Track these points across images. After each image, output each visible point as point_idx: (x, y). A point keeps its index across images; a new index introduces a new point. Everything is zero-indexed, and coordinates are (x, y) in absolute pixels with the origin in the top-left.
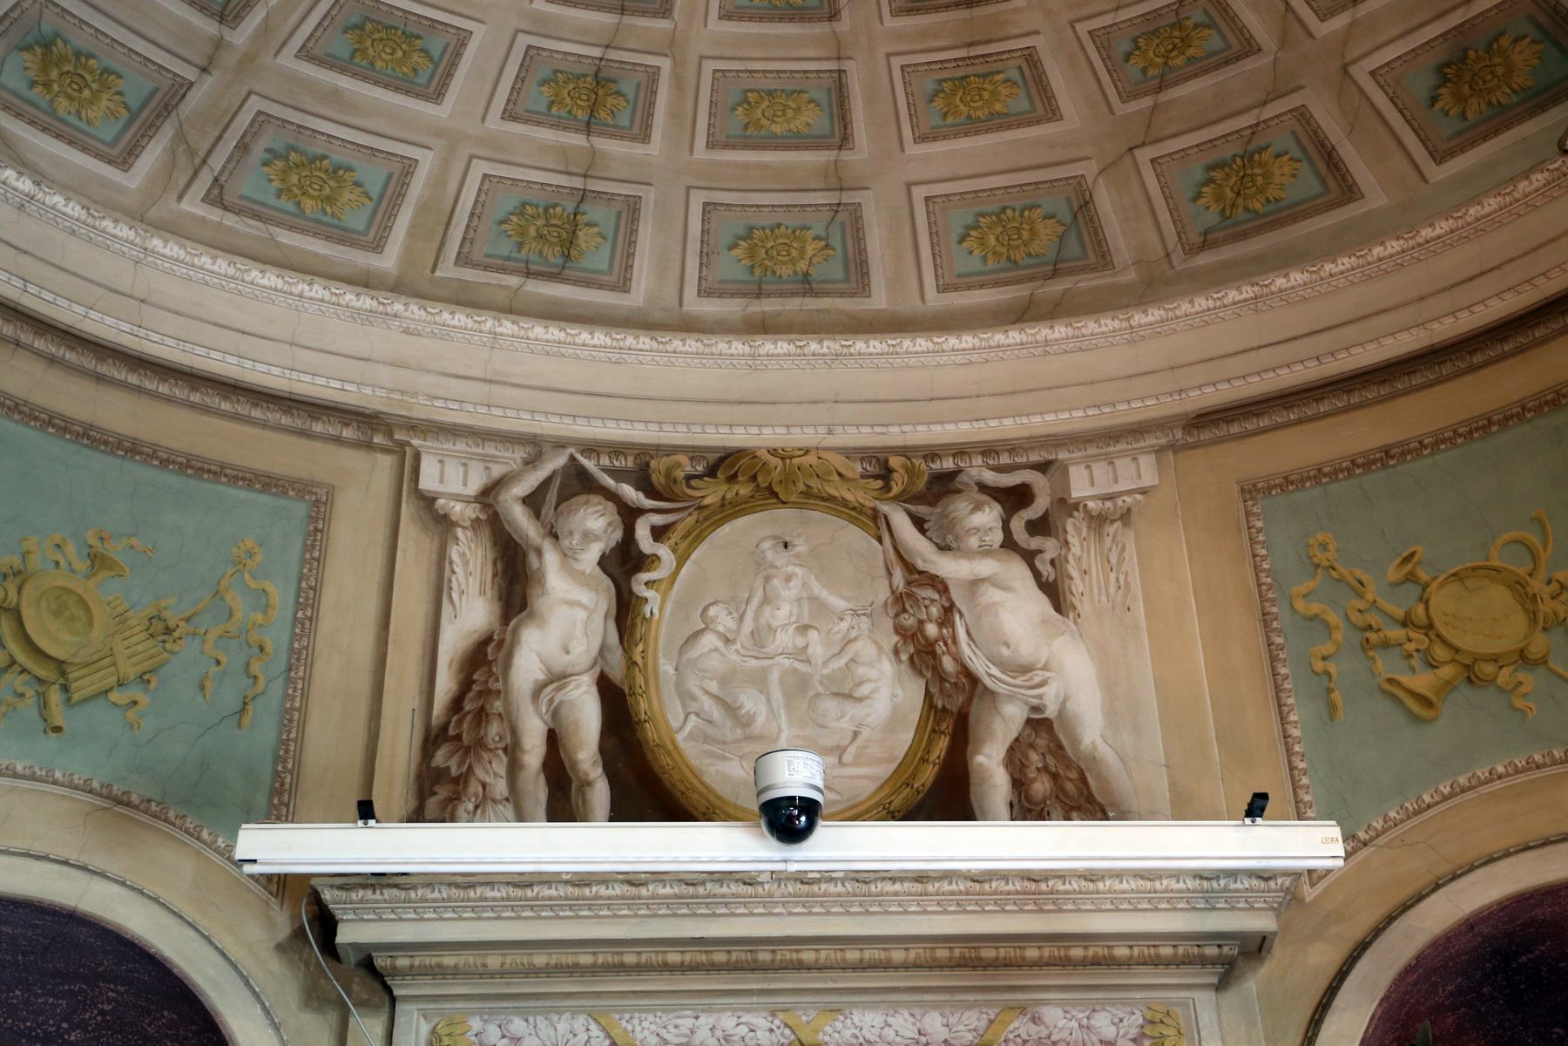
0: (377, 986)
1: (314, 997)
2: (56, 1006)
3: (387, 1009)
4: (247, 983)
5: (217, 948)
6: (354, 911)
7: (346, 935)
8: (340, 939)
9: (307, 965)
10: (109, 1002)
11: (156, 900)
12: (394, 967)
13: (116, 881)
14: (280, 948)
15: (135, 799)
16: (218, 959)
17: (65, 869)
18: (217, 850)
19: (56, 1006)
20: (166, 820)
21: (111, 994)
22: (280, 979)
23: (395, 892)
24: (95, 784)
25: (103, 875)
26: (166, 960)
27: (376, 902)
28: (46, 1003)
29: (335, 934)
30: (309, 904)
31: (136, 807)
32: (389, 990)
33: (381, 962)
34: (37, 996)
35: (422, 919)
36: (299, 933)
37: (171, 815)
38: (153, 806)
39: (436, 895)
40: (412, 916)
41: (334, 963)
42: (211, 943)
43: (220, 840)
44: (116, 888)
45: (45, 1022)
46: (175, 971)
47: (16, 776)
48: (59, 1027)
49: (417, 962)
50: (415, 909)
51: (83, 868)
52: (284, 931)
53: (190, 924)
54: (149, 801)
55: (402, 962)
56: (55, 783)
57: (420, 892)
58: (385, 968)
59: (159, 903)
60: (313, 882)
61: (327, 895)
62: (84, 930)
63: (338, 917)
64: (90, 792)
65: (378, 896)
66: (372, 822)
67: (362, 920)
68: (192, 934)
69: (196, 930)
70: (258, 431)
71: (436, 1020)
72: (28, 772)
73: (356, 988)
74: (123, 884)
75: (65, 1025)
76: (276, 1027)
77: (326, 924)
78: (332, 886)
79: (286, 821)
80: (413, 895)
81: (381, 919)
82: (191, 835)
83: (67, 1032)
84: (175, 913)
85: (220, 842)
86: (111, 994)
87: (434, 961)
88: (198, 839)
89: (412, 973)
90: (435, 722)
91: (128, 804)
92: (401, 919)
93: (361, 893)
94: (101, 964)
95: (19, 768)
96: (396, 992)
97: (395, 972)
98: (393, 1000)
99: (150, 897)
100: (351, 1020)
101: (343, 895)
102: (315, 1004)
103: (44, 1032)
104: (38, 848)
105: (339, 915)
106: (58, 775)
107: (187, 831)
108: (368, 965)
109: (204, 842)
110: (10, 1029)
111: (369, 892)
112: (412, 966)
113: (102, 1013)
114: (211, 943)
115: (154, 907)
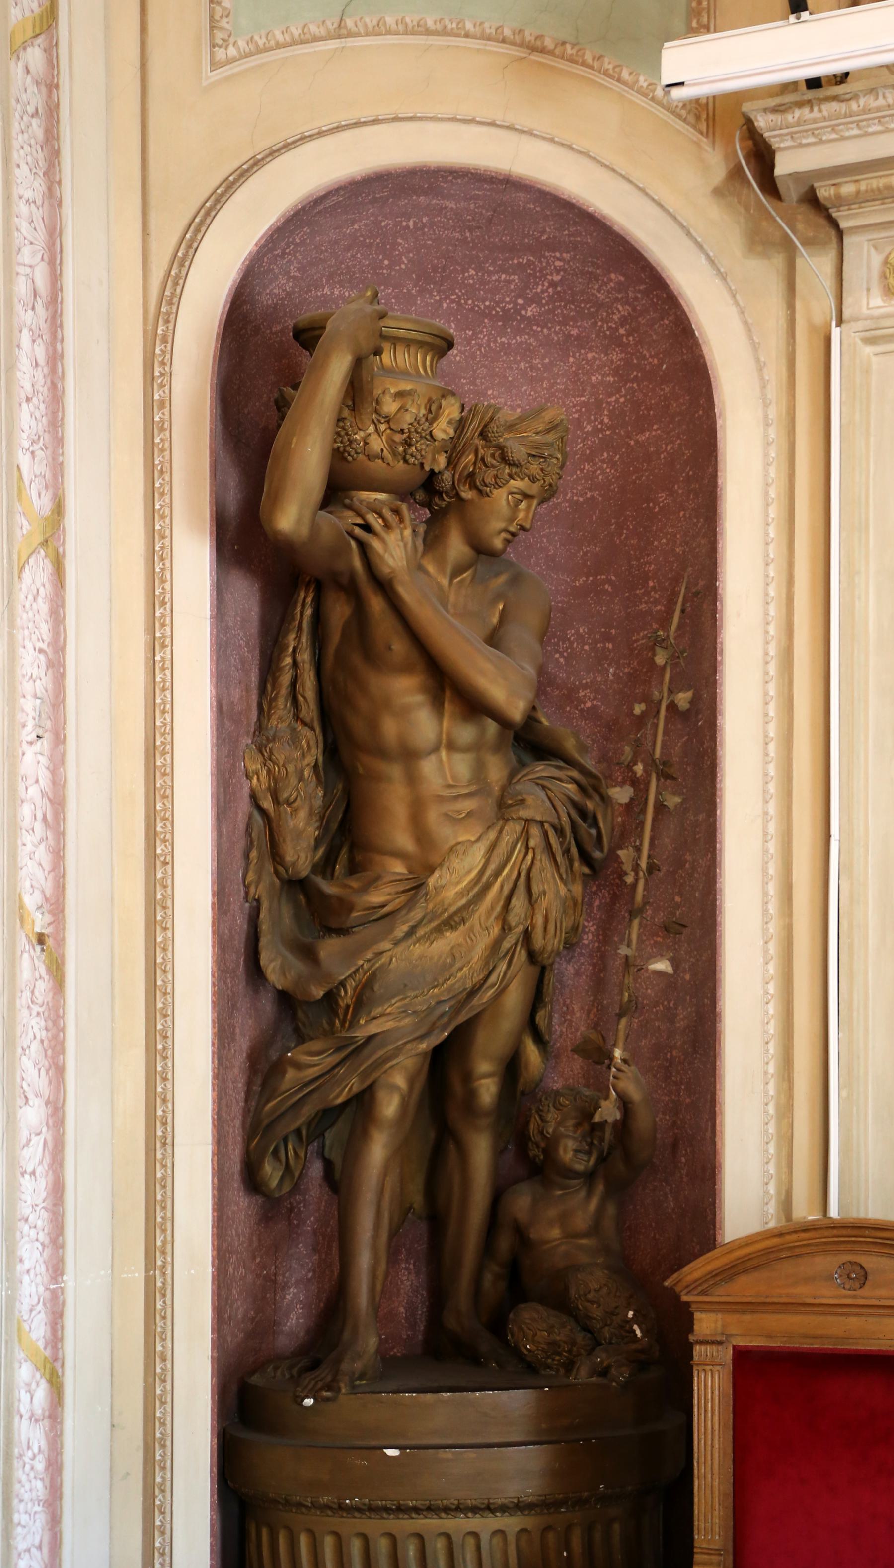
0: (822, 221)
1: (759, 241)
2: (509, 282)
3: (835, 240)
4: (689, 234)
5: (653, 200)
6: (792, 135)
7: (784, 166)
8: (779, 171)
9: (747, 208)
10: (558, 272)
11: (586, 154)
12: (838, 197)
13: (544, 138)
14: (718, 192)
15: (549, 43)
16: (656, 210)
17: (493, 130)
18: (640, 92)
19: (509, 282)
20: (584, 64)
21: (558, 264)
22: (721, 225)
23: (835, 106)
24: (507, 32)
25: (530, 133)
26: (605, 217)
27: (815, 121)
28: (498, 280)
29: (772, 167)
30: (742, 139)
31: (551, 53)
32: (834, 224)
33: (824, 192)
34: (490, 273)
35: (867, 134)
36: (736, 173)
37: (588, 57)
38: (569, 50)
39: (881, 102)
40: (856, 132)
41: (776, 202)
42: (647, 194)
43: (641, 79)
44: (545, 146)
45: (502, 301)
46: (616, 228)
47: (428, 32)
48: (516, 304)
49: (863, 186)
50: (858, 123)
51: (510, 128)
52: (719, 172)
53: (623, 177)
54: (564, 43)
55: (847, 189)
56: (467, 36)
57: (862, 102)
58: (829, 199)
59: (590, 157)
60: (747, 107)
61: (762, 122)
62: (522, 195)
63: (775, 146)
64: (504, 41)
65: (816, 114)
66: (805, 15)
67: (801, 145)
68: (627, 186)
69: (631, 182)
70: (69, 1320)
71: (888, 250)
72: (439, 27)
73: (800, 226)
74: (552, 140)
75: (520, 301)
76: (723, 277)
77: (762, 156)
78: (765, 110)
79: (708, 31)
80: (854, 106)
81: (821, 142)
82: (611, 77)
83: (524, 307)
84: (607, 167)
85: (643, 82)
86: (558, 263)
87: (882, 182)
88: (619, 80)
89: (859, 199)
90: (452, 1146)
91: (543, 51)
92: (843, 138)
93: (797, 113)
94: (544, 232)
95: (430, 23)
96: (843, 225)
97: (841, 201)
98: (840, 234)
99: (580, 152)
100: (799, 262)
101: (777, 118)
102: (760, 249)
103: (503, 309)
104: (465, 111)
105: (775, 143)
106: (469, 26)
107: (606, 73)
108: (812, 200)
109: (625, 83)
110: (472, 310)
111: (806, 110)
112: (858, 192)
113: (553, 284)
114: (647, 194)
115: (585, 161)
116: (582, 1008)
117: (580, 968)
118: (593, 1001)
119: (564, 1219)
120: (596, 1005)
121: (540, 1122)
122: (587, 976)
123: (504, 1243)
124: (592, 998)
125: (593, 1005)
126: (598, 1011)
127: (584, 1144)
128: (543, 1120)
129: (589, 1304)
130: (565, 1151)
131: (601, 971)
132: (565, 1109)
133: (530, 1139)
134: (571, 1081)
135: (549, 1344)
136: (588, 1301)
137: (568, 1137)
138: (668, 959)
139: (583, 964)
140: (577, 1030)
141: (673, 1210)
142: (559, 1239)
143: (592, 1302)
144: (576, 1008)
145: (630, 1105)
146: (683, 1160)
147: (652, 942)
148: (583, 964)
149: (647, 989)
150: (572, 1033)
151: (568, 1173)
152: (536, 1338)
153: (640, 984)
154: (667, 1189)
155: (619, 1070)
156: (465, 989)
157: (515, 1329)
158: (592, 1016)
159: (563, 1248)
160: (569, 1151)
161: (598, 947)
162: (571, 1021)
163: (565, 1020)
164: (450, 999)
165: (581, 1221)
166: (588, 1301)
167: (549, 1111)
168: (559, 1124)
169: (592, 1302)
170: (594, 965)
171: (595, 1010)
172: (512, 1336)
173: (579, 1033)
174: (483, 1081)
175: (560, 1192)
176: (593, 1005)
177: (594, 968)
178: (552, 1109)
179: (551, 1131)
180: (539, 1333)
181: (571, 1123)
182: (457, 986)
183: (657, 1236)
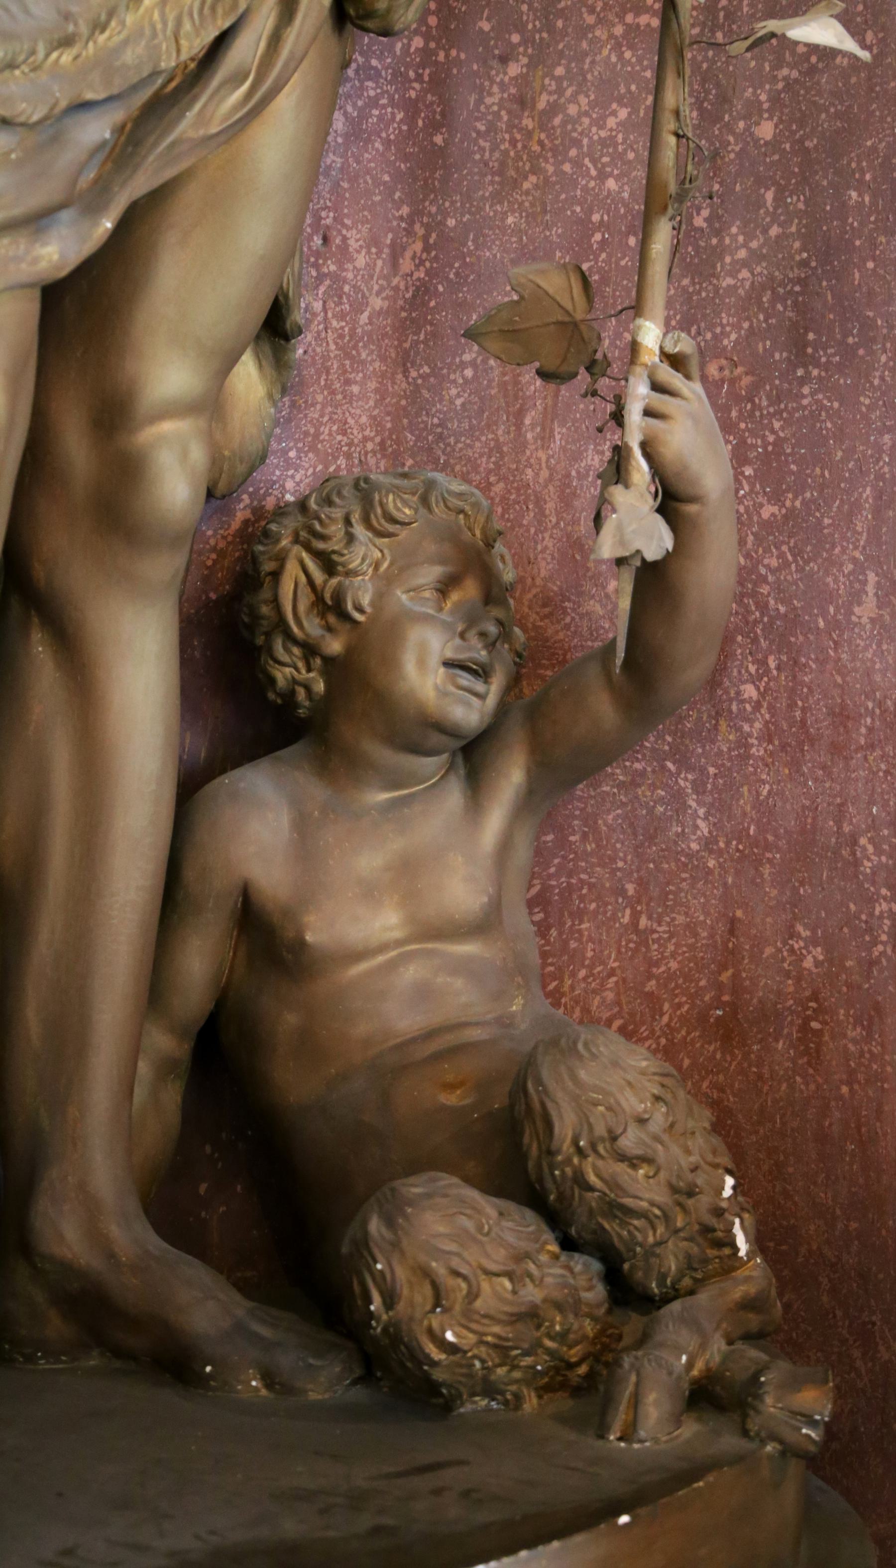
90: (39, 649)
116: (374, 241)
117: (363, 115)
118: (411, 220)
119: (408, 874)
120: (420, 230)
121: (318, 576)
122: (387, 143)
123: (200, 961)
124: (405, 210)
125: (409, 232)
126: (427, 248)
127: (474, 640)
128: (329, 565)
129: (621, 1168)
130: (421, 663)
131: (433, 126)
132: (404, 534)
133: (281, 625)
134: (342, 462)
135: (517, 1318)
136: (622, 1157)
137: (425, 618)
138: (837, 17)
139: (374, 102)
140: (358, 307)
141: (708, 843)
142: (399, 943)
143: (633, 1162)
144: (355, 238)
145: (692, 509)
146: (750, 691)
147: (619, 30)
148: (374, 102)
149: (602, 176)
150: (342, 316)
151: (418, 732)
152: (478, 1304)
153: (577, 163)
154: (685, 782)
155: (657, 387)
156: (155, 74)
157: (401, 1274)
158: (406, 264)
159: (411, 973)
160: (430, 668)
161: (425, 52)
162: (337, 279)
163: (320, 278)
164: (110, 99)
165: (462, 890)
166: (622, 1157)
167: (350, 538)
168: (386, 582)
169: (633, 1162)
170: (412, 108)
171: (418, 246)
172: (390, 1301)
173: (364, 318)
174: (167, 427)
175: (384, 796)
176: (409, 232)
177: (411, 119)
178: (359, 530)
179: (366, 601)
180: (485, 1286)
181: (430, 574)
182: (129, 56)
183: (643, 922)
